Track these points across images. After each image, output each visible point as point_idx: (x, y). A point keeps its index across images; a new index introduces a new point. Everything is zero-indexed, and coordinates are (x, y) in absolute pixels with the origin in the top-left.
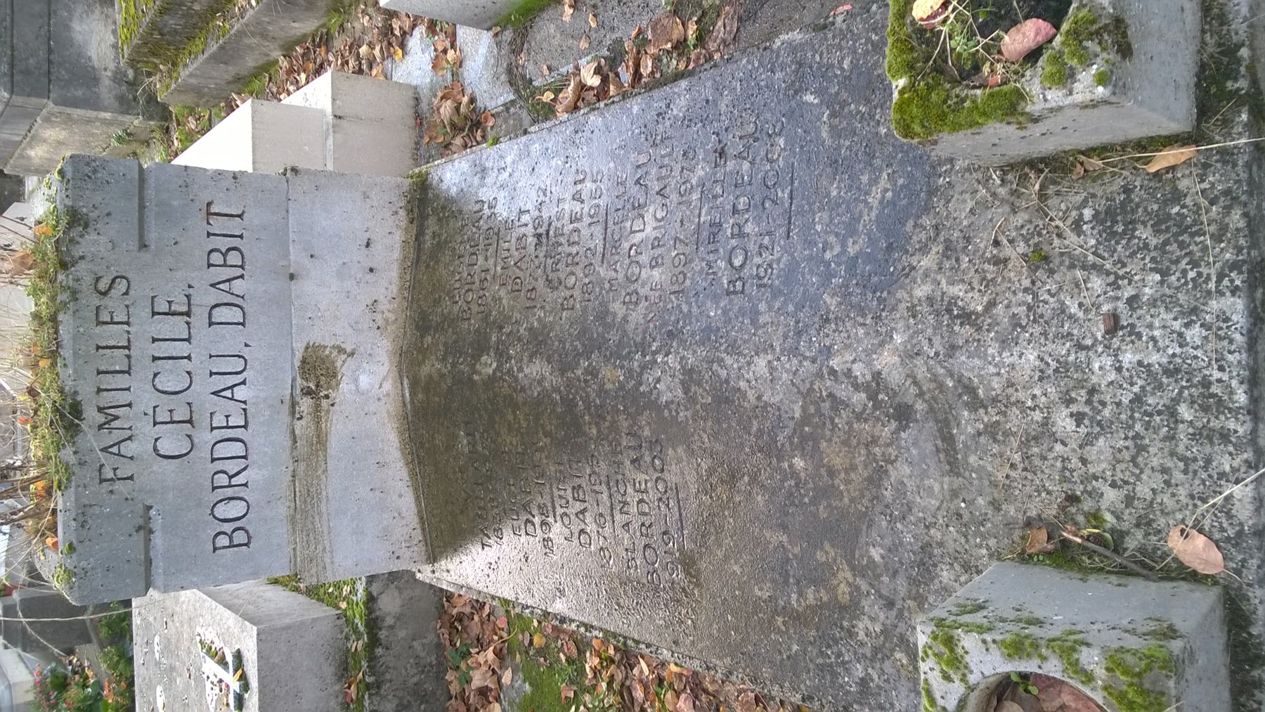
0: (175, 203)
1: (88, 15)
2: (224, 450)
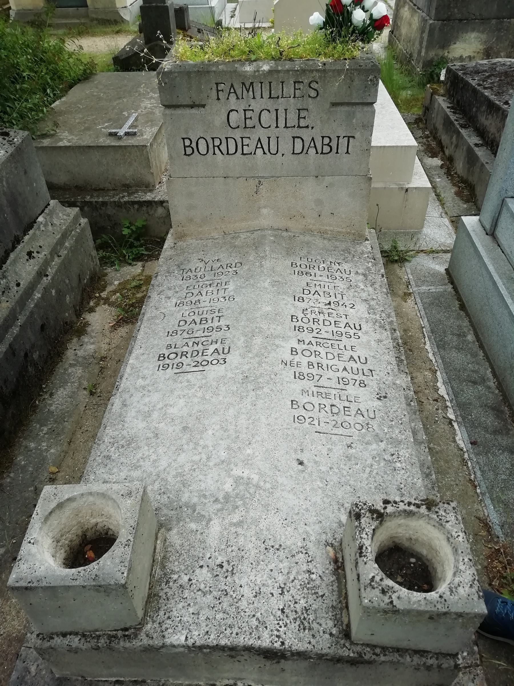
0: (354, 121)
1: (479, 41)
2: (231, 143)
